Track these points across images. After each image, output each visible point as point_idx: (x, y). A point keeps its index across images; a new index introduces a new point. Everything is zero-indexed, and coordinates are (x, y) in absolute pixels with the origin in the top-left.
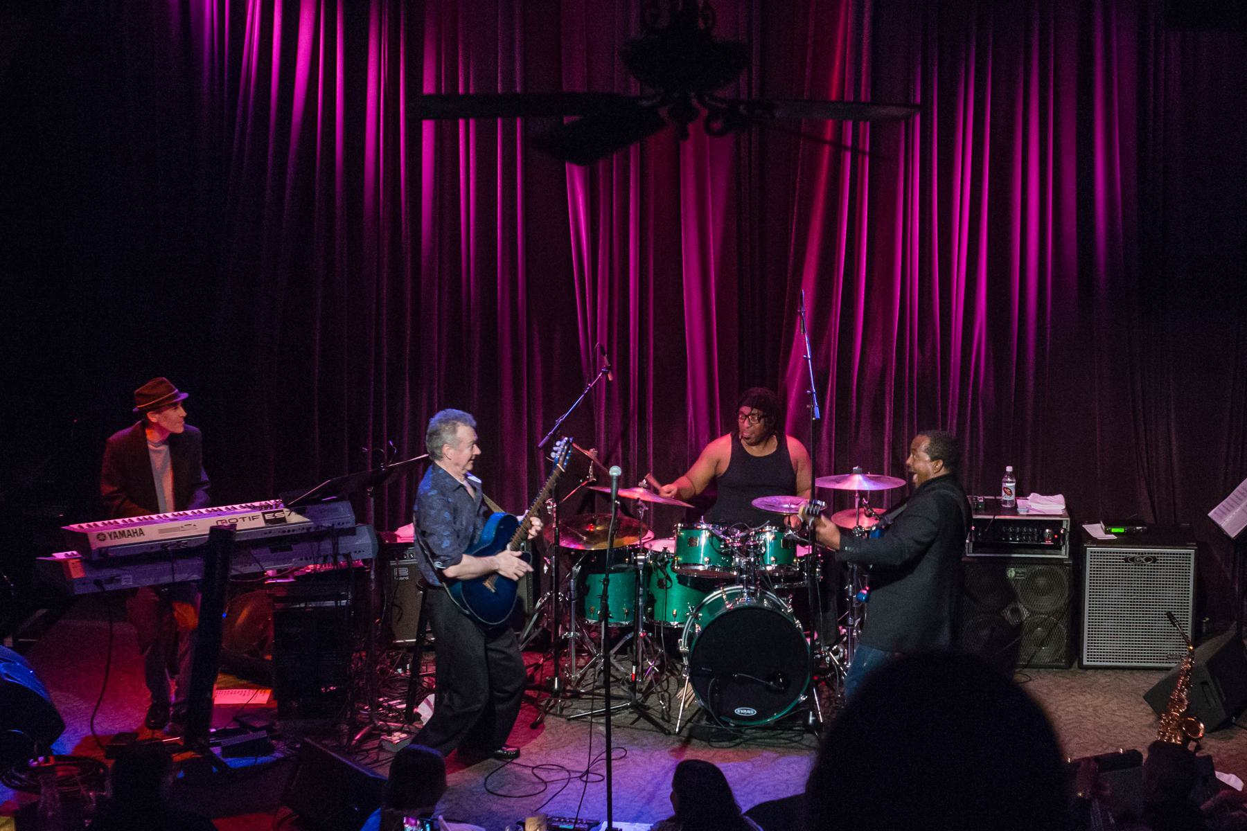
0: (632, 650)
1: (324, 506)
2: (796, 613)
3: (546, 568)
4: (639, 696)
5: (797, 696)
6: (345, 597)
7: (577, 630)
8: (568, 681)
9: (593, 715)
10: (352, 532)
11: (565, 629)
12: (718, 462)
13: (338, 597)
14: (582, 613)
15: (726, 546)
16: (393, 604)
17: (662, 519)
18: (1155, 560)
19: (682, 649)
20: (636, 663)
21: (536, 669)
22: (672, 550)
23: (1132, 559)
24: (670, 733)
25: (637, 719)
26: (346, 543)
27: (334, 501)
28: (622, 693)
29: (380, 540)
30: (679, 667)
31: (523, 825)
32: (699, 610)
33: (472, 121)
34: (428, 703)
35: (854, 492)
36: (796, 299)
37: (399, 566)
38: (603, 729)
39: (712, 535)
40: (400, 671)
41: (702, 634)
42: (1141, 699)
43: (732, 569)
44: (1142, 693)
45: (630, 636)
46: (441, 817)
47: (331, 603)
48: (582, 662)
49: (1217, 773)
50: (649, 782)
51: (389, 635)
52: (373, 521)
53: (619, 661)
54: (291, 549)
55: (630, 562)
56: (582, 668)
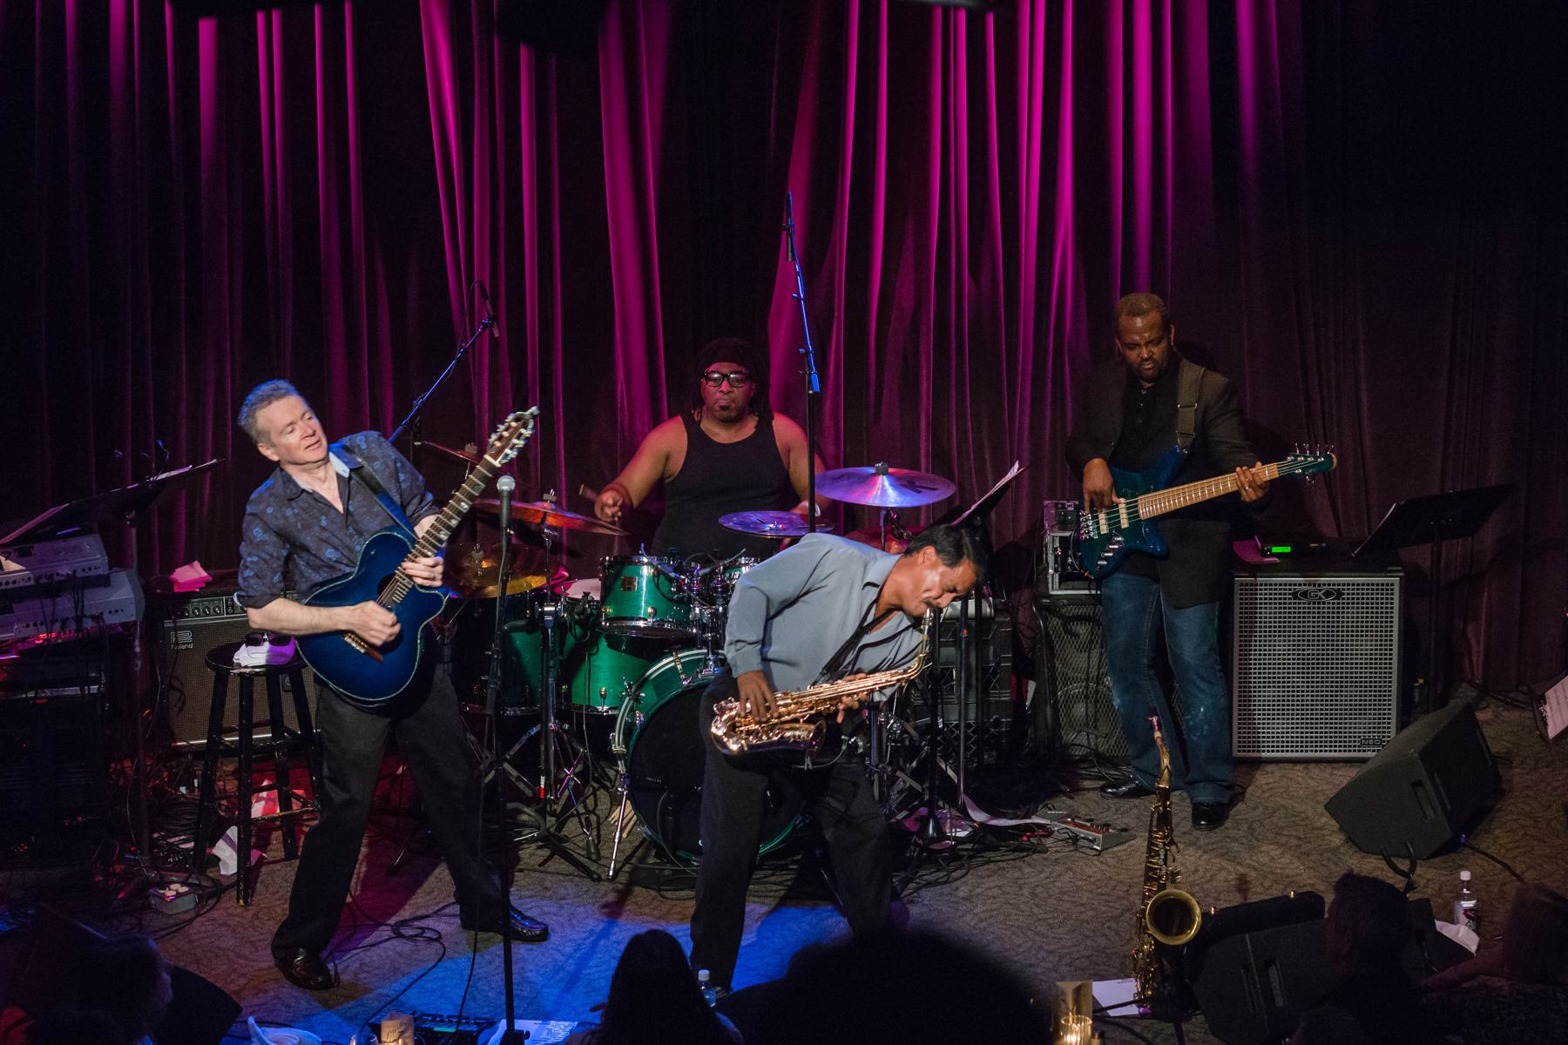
1: (62, 544)
4: (551, 820)
6: (96, 681)
10: (104, 582)
12: (668, 457)
13: (85, 681)
15: (680, 590)
16: (171, 686)
17: (577, 553)
18: (1339, 595)
23: (1305, 594)
24: (599, 879)
26: (96, 600)
27: (73, 535)
29: (147, 589)
30: (611, 773)
31: (377, 1030)
32: (639, 688)
33: (275, 15)
34: (229, 841)
37: (176, 629)
39: (658, 573)
40: (183, 790)
41: (646, 726)
42: (1321, 809)
43: (690, 624)
44: (1323, 799)
45: (535, 730)
46: (251, 1020)
47: (73, 691)
49: (1438, 924)
50: (570, 956)
51: (164, 732)
52: (135, 564)
54: (11, 611)
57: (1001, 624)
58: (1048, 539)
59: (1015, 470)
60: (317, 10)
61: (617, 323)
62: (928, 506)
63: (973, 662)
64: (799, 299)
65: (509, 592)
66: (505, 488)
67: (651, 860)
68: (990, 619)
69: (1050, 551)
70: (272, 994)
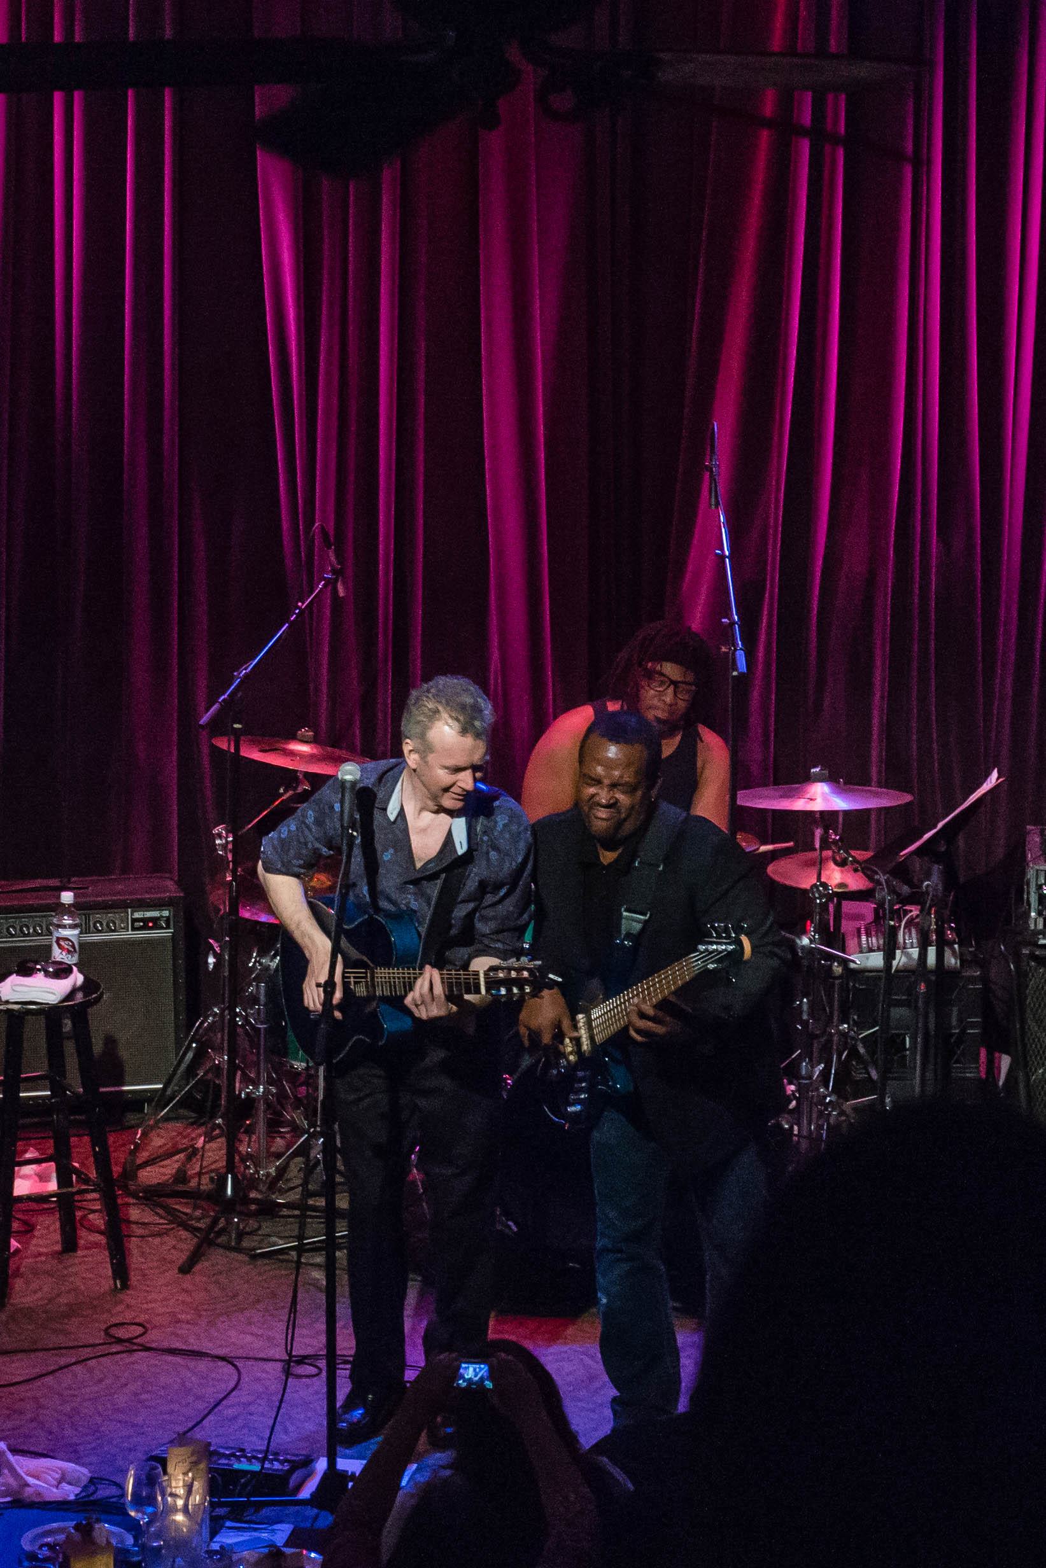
3: (211, 960)
7: (271, 1081)
8: (253, 1183)
11: (246, 1080)
21: (189, 1158)
36: (702, 440)
48: (280, 1142)
56: (278, 1156)
57: (972, 980)
58: (1030, 874)
59: (994, 778)
60: (102, 1090)
61: (492, 581)
62: (879, 810)
63: (932, 1026)
64: (723, 557)
66: (348, 777)
68: (954, 973)
69: (1033, 889)
70: (29, 1416)
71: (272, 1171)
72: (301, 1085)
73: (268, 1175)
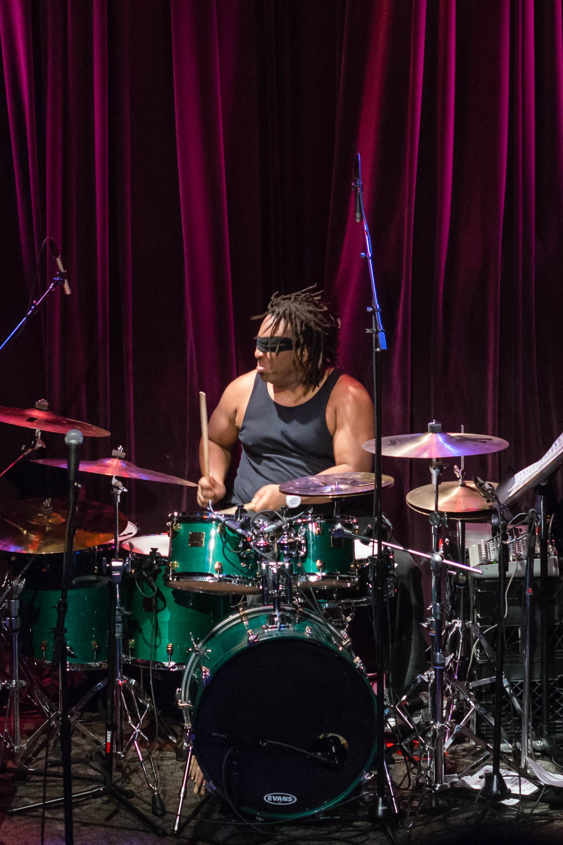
0: (105, 705)
2: (355, 648)
5: (359, 773)
9: (45, 807)
12: (236, 412)
14: (28, 650)
19: (183, 704)
20: (112, 727)
22: (164, 552)
25: (116, 812)
28: (91, 772)
35: (429, 461)
38: (61, 827)
53: (86, 723)
55: (100, 573)
62: (494, 454)
64: (366, 259)
65: (76, 548)
66: (73, 442)
67: (216, 816)
68: (554, 579)
71: (24, 746)
72: (47, 676)
73: (21, 749)
